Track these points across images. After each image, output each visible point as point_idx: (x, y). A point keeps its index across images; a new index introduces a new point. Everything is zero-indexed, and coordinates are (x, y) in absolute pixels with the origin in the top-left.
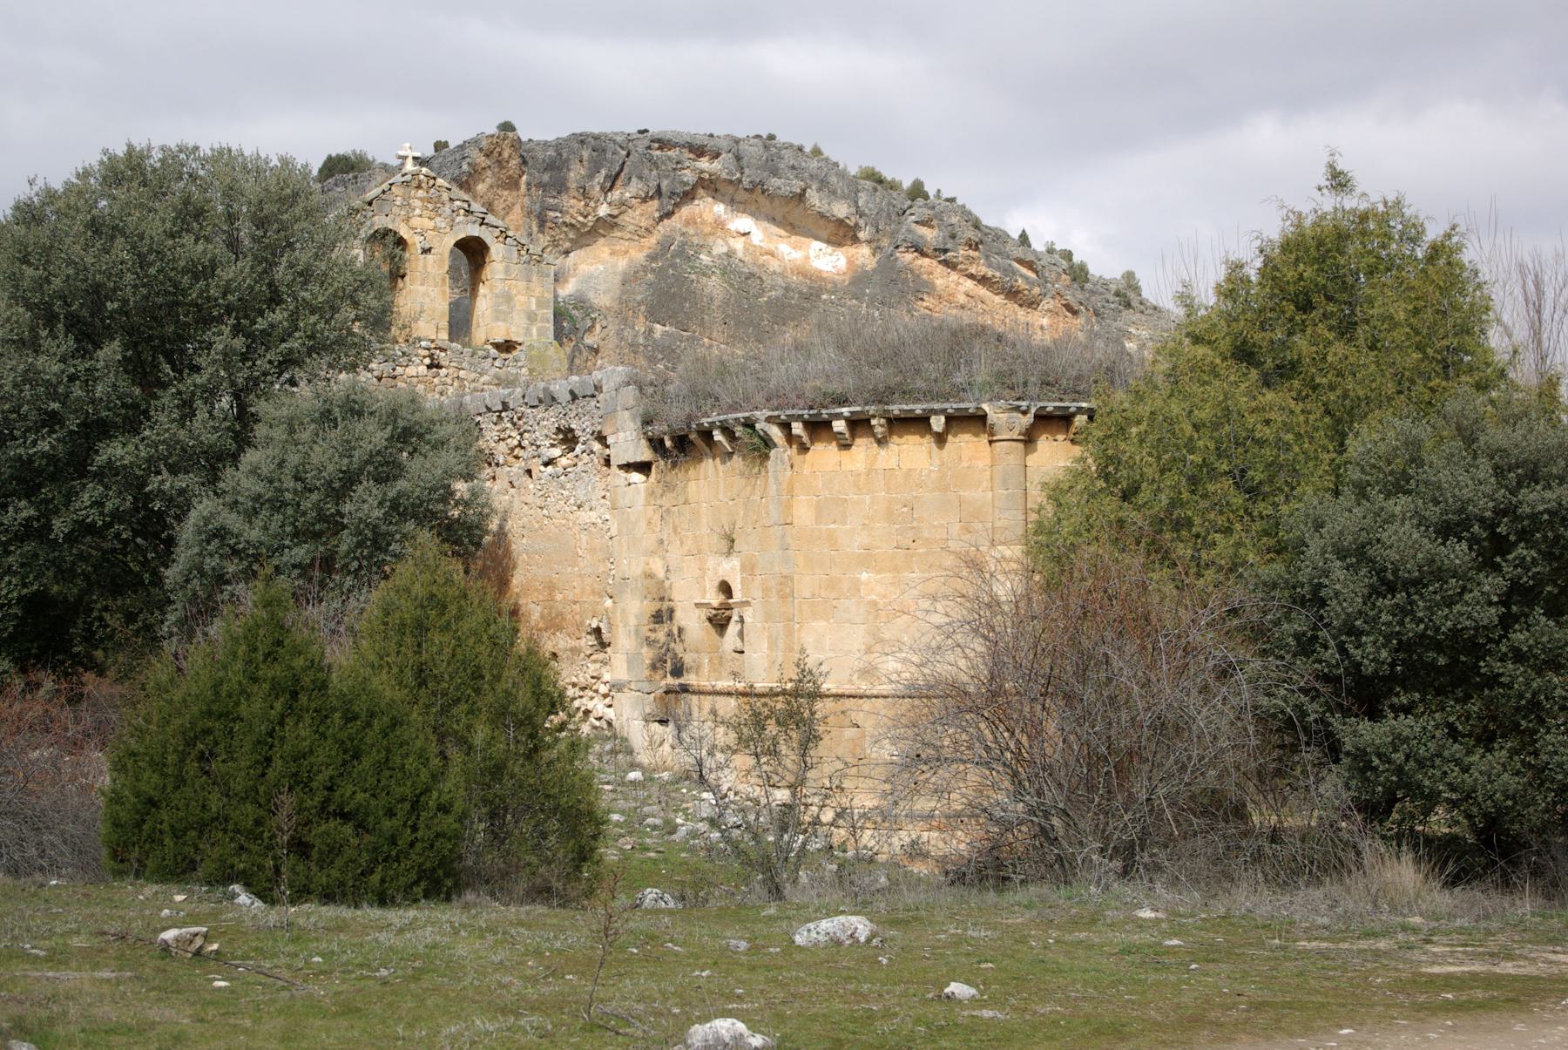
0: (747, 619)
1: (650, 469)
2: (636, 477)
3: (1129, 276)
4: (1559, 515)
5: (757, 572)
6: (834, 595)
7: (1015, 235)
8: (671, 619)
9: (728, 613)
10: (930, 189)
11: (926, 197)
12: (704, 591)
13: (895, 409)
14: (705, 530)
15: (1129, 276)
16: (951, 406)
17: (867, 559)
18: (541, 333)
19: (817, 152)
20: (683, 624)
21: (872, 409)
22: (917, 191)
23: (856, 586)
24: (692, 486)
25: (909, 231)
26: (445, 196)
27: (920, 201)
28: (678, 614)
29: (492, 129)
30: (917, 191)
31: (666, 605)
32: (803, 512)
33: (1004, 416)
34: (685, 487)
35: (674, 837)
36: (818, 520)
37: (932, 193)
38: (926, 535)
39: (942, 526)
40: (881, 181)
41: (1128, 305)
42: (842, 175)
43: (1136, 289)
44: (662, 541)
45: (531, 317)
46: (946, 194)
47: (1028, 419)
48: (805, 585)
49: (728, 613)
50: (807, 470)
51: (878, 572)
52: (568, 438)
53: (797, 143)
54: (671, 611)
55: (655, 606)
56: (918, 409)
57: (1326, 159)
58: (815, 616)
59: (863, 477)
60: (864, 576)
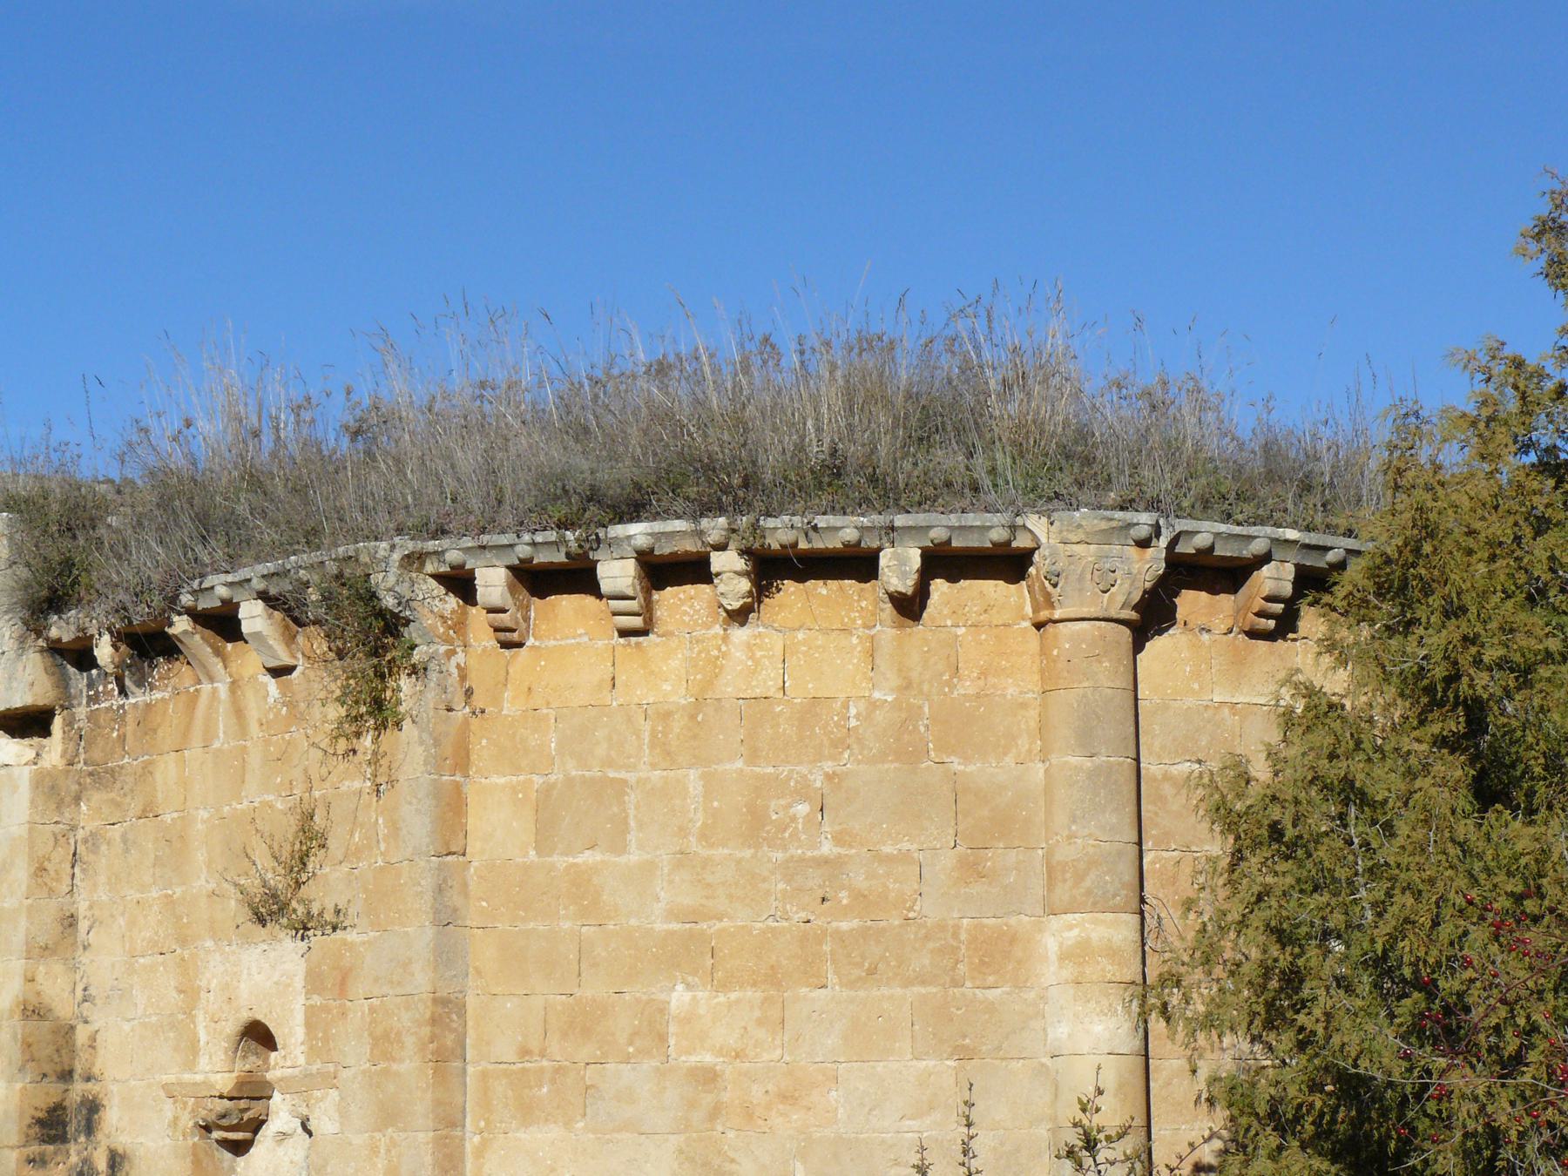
0: (324, 1124)
1: (45, 732)
4: (1531, 1172)
5: (358, 989)
6: (585, 1053)
8: (90, 1129)
9: (256, 1109)
12: (192, 1050)
13: (781, 531)
14: (203, 882)
16: (941, 526)
17: (690, 952)
20: (122, 1141)
21: (715, 527)
23: (653, 1030)
24: (167, 770)
28: (112, 1118)
31: (78, 1089)
32: (497, 823)
33: (1088, 552)
34: (147, 770)
35: (411, 546)
36: (544, 839)
38: (860, 880)
39: (905, 857)
44: (71, 921)
48: (498, 1029)
49: (256, 1109)
50: (510, 706)
51: (724, 986)
54: (92, 1108)
55: (50, 1093)
58: (528, 1113)
59: (678, 724)
60: (679, 998)
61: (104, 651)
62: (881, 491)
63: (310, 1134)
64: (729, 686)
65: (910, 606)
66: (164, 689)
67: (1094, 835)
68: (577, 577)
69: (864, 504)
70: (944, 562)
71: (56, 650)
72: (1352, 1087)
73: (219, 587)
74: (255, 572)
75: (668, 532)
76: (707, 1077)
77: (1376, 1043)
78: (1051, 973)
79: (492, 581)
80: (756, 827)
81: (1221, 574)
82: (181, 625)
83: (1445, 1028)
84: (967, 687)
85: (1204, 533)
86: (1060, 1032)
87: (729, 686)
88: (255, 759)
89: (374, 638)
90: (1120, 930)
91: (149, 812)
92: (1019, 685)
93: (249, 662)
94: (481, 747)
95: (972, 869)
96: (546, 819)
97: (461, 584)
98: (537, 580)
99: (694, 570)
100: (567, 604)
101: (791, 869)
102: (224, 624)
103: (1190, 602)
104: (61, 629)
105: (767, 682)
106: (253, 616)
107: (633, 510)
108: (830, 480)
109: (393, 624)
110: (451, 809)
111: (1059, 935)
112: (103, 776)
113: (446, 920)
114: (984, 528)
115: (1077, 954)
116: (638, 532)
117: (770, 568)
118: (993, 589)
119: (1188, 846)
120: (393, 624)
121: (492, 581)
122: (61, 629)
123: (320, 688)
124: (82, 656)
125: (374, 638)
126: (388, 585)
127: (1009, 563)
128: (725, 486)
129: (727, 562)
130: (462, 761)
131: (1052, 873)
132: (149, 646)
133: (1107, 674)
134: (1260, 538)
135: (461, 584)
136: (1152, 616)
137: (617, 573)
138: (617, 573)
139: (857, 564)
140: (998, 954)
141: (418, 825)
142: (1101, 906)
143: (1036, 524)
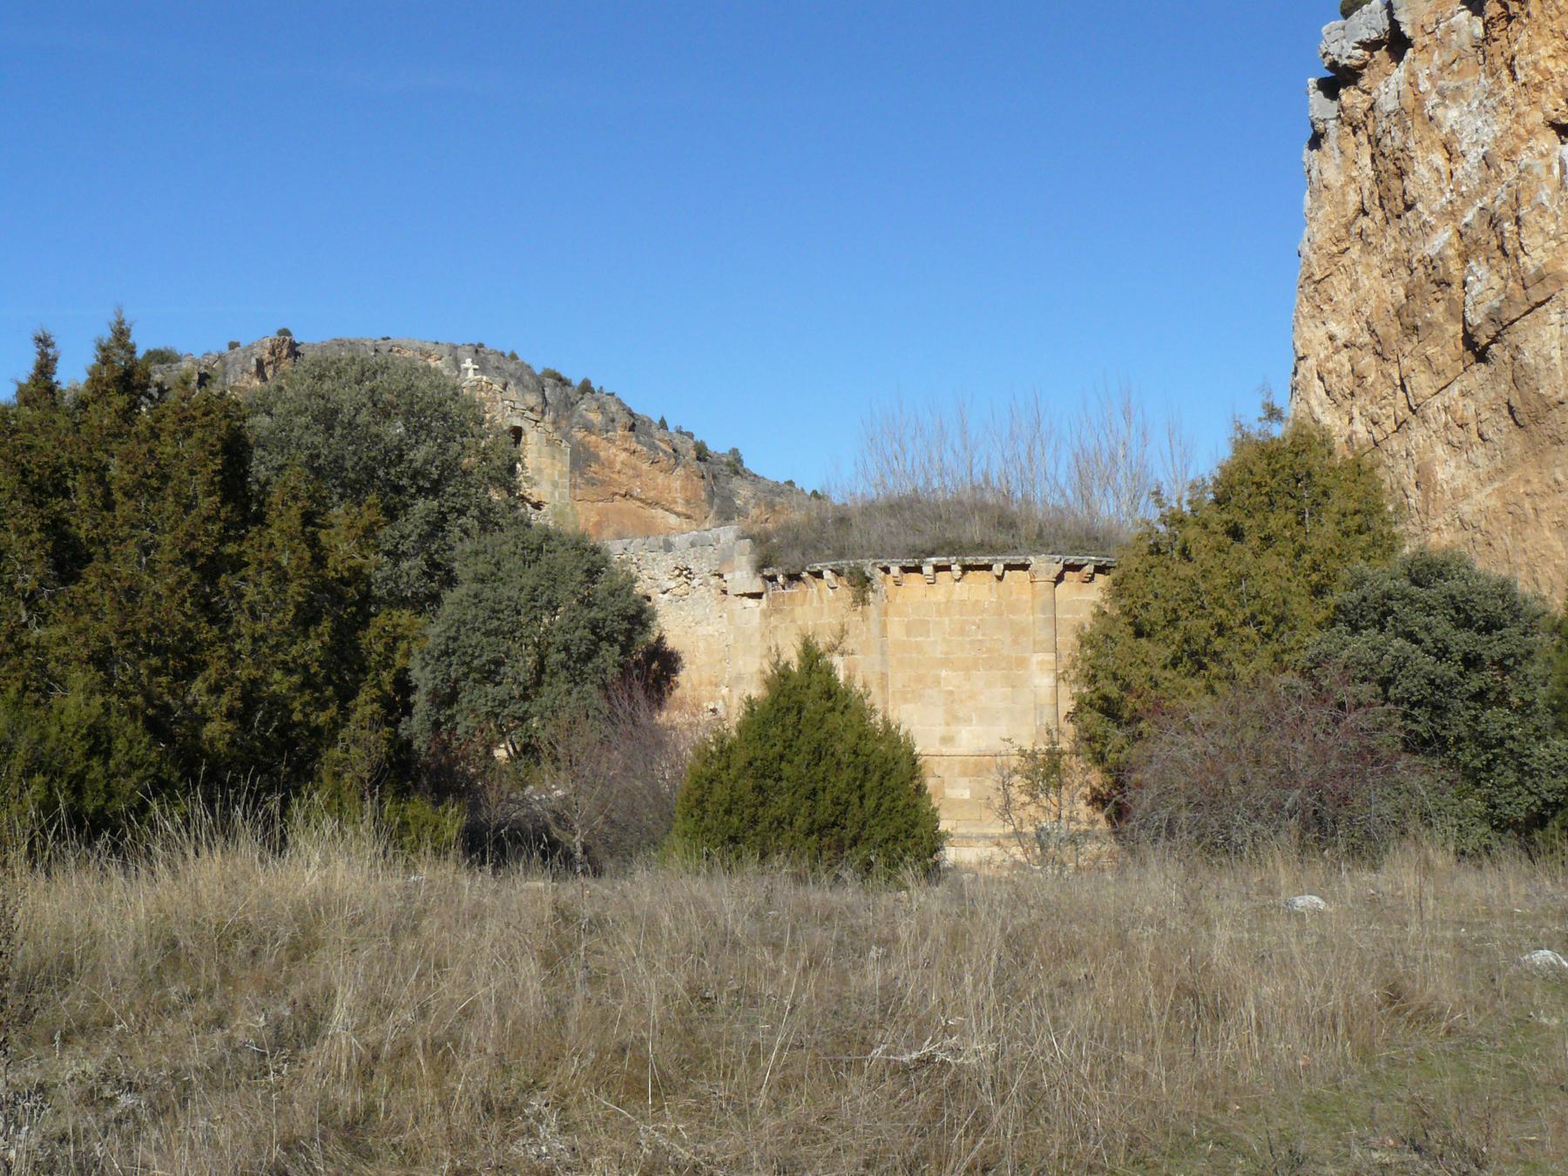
2: (751, 602)
3: (735, 452)
7: (657, 421)
10: (595, 386)
11: (593, 392)
13: (969, 560)
15: (735, 452)
16: (1009, 559)
17: (946, 662)
18: (561, 496)
19: (514, 357)
22: (586, 387)
25: (581, 416)
26: (499, 397)
27: (588, 395)
29: (273, 335)
30: (586, 387)
32: (896, 629)
36: (908, 633)
37: (596, 389)
40: (560, 379)
41: (737, 473)
42: (532, 375)
43: (740, 461)
45: (555, 485)
46: (607, 390)
47: (1060, 567)
50: (898, 600)
52: (685, 572)
53: (499, 350)
56: (985, 560)
57: (113, 319)
58: (905, 701)
60: (944, 673)
61: (780, 579)
62: (993, 549)
63: (44, 342)
64: (955, 597)
65: (1000, 578)
66: (796, 589)
67: (1044, 634)
68: (918, 569)
69: (989, 553)
70: (1008, 567)
71: (765, 577)
72: (1105, 698)
73: (818, 567)
74: (830, 564)
75: (943, 560)
76: (951, 693)
77: (1113, 690)
78: (1034, 667)
79: (895, 570)
80: (962, 632)
81: (1076, 568)
82: (805, 575)
83: (1126, 687)
84: (1014, 597)
85: (1072, 559)
86: (1037, 681)
87: (955, 597)
88: (826, 610)
89: (862, 583)
90: (1051, 657)
91: (793, 621)
92: (1027, 597)
93: (822, 584)
94: (891, 610)
95: (1015, 642)
96: (909, 629)
97: (886, 570)
98: (905, 570)
99: (947, 568)
100: (913, 575)
101: (971, 642)
102: (819, 575)
103: (1068, 574)
104: (767, 572)
105: (964, 597)
106: (827, 574)
107: (932, 554)
108: (980, 547)
109: (868, 580)
110: (884, 626)
111: (1037, 658)
112: (777, 611)
113: (883, 654)
114: (1020, 560)
115: (1041, 663)
116: (934, 560)
117: (966, 568)
118: (1020, 572)
119: (1068, 640)
120: (868, 580)
121: (895, 570)
122: (767, 572)
123: (845, 592)
124: (773, 579)
125: (862, 583)
126: (868, 571)
127: (1025, 567)
128: (954, 548)
129: (956, 568)
130: (886, 614)
131: (1035, 642)
132: (793, 578)
133: (1048, 595)
134: (1085, 559)
135: (886, 570)
136: (1059, 579)
137: (928, 569)
138: (928, 569)
139: (988, 568)
140: (1022, 663)
141: (876, 630)
142: (1045, 651)
143: (1032, 558)
